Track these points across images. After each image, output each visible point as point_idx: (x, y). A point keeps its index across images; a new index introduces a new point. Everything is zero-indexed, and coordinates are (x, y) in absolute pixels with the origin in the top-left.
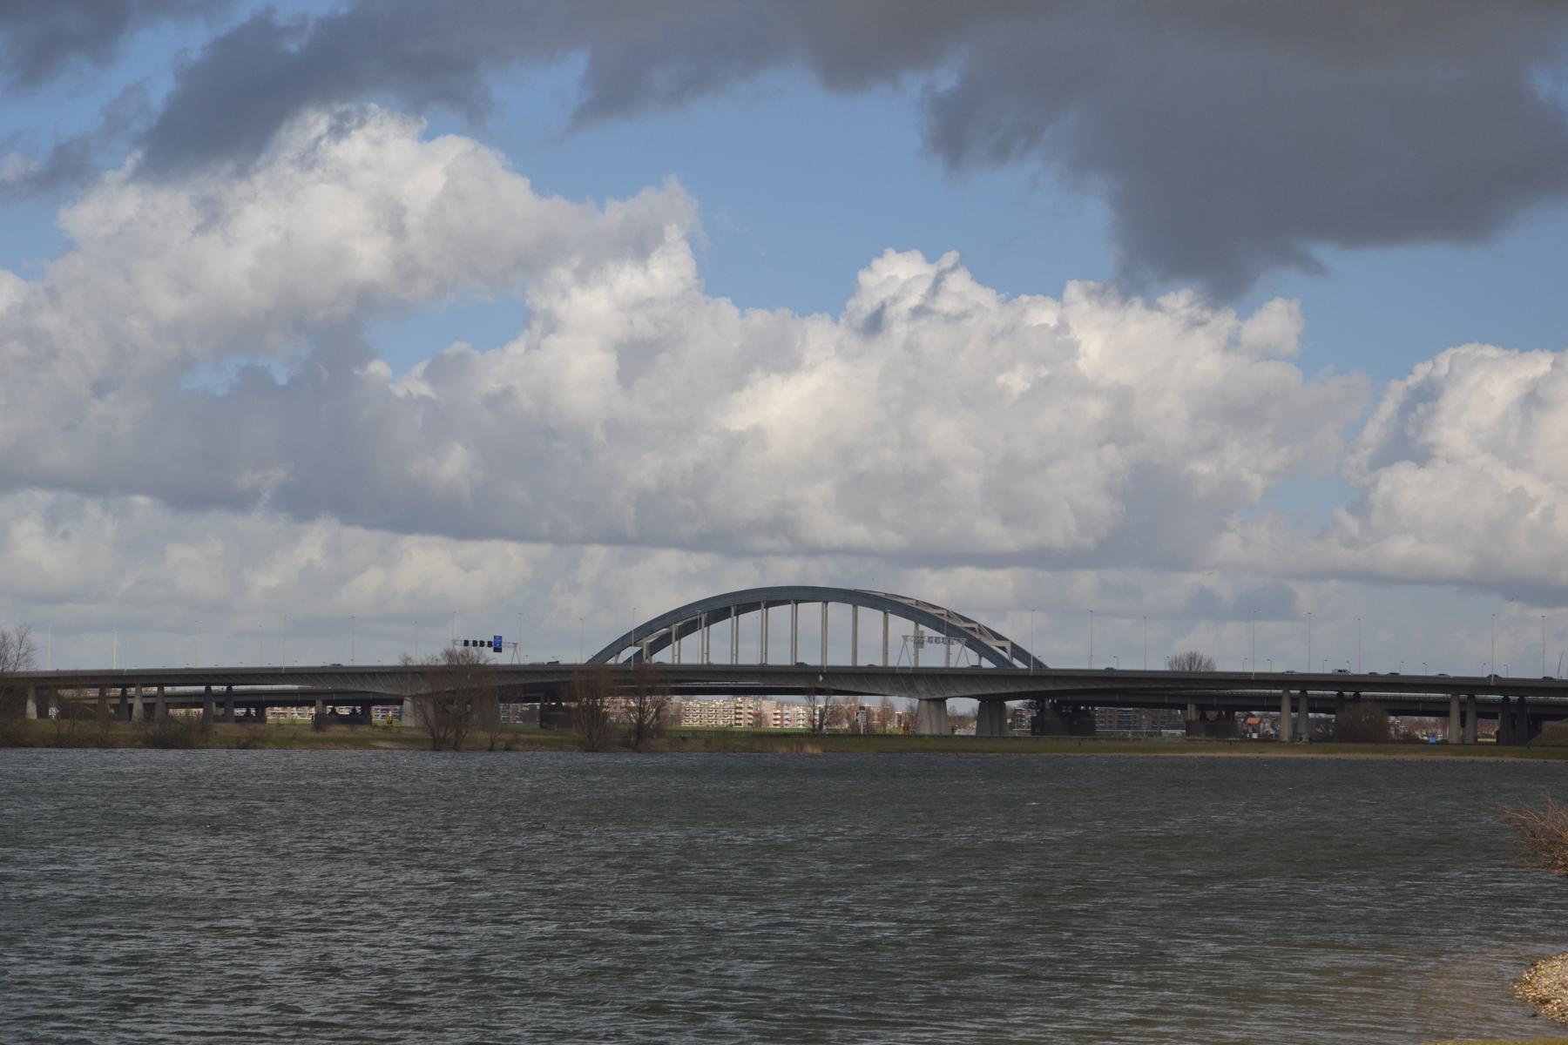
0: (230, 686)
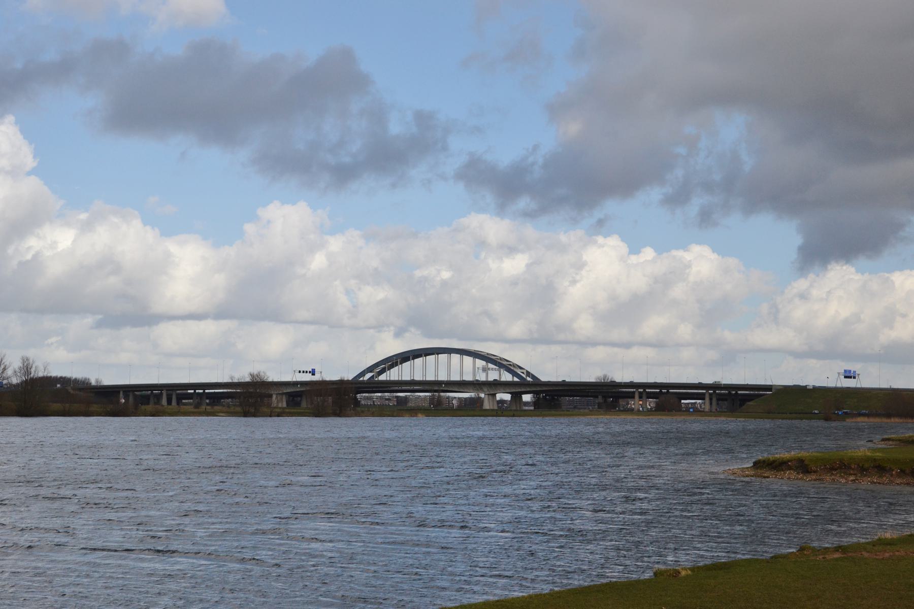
0: (204, 390)
